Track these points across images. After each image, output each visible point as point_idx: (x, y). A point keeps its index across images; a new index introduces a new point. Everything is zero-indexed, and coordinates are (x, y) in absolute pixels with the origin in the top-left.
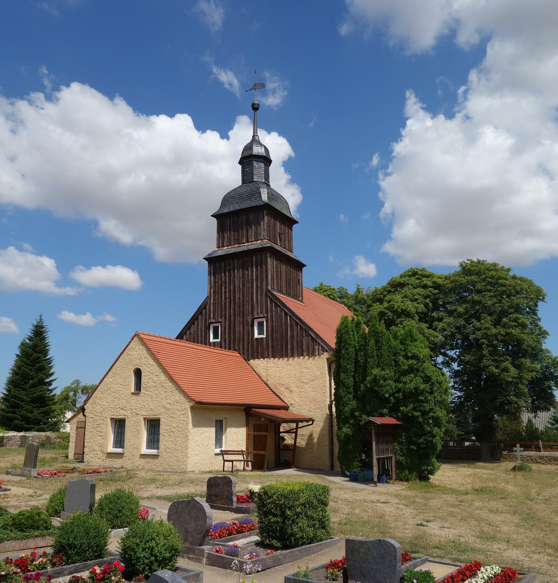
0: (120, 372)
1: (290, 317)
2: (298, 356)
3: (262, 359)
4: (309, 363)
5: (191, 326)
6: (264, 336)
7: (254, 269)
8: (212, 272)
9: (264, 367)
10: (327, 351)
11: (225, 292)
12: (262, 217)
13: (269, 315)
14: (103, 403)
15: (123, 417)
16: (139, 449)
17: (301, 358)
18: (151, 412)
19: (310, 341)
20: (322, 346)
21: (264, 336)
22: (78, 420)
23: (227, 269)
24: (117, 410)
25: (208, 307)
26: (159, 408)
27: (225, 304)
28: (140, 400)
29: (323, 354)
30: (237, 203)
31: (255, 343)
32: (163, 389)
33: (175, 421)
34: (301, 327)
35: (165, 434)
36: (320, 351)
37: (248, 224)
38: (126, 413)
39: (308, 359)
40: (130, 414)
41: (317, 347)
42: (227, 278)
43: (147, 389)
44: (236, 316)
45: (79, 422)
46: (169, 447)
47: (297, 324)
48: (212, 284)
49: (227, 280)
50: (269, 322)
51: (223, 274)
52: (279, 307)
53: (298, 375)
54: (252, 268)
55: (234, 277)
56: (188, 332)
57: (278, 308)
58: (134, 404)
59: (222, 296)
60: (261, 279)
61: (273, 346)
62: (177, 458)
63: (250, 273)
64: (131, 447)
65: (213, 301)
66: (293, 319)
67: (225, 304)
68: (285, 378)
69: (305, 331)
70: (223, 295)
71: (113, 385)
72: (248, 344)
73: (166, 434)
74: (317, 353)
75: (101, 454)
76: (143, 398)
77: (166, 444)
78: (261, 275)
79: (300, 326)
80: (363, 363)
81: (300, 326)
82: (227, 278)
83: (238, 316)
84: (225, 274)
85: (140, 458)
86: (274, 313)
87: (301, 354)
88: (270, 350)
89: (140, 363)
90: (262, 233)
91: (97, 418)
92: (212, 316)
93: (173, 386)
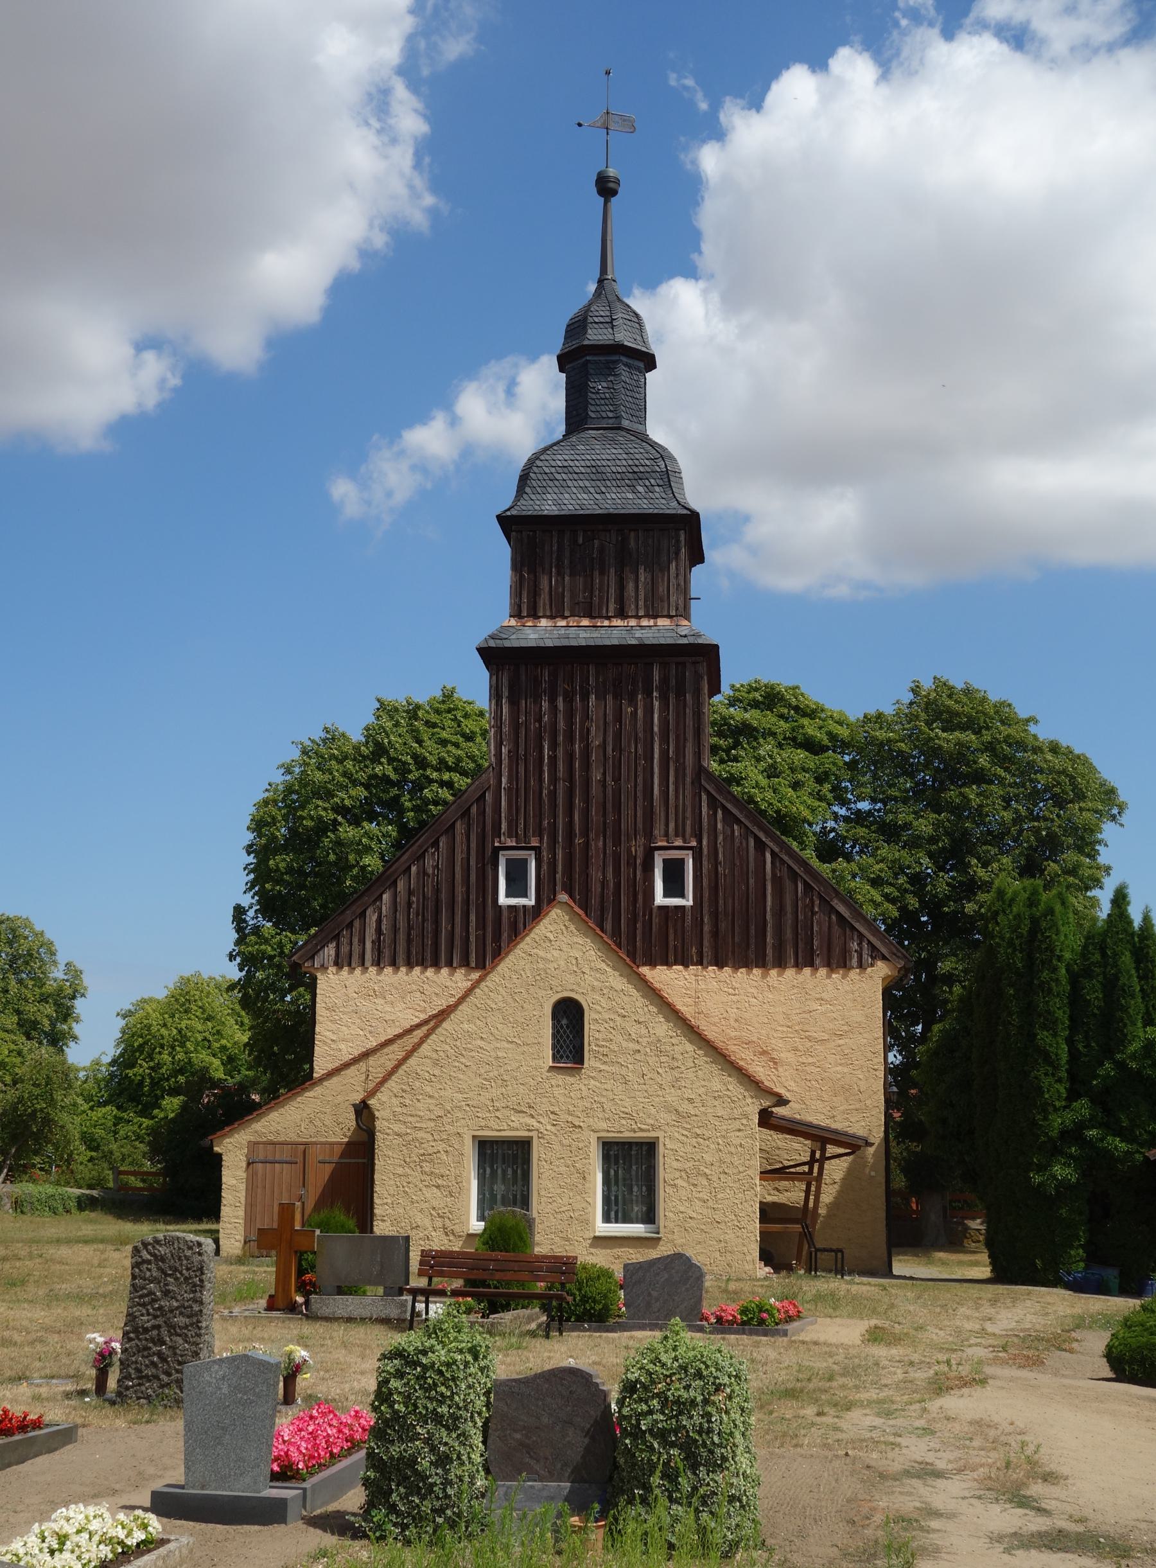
0: (501, 1004)
1: (773, 853)
2: (798, 966)
3: (680, 968)
4: (830, 987)
5: (426, 850)
6: (688, 902)
7: (656, 704)
8: (506, 693)
9: (687, 989)
10: (884, 958)
11: (553, 760)
12: (672, 549)
13: (705, 842)
14: (442, 1093)
15: (526, 1134)
16: (587, 1222)
17: (807, 971)
18: (624, 1122)
19: (836, 929)
20: (869, 942)
21: (688, 902)
22: (252, 1139)
23: (560, 690)
24: (498, 1114)
25: (489, 797)
26: (653, 1111)
27: (553, 794)
28: (583, 1088)
29: (872, 965)
30: (584, 489)
31: (655, 920)
32: (663, 1059)
33: (712, 1146)
34: (807, 885)
35: (676, 1182)
36: (865, 956)
37: (625, 561)
38: (535, 1124)
39: (829, 976)
40: (549, 1127)
41: (855, 946)
42: (561, 717)
43: (605, 1059)
44: (592, 835)
45: (258, 1143)
46: (694, 1215)
47: (794, 876)
48: (505, 729)
49: (561, 725)
50: (705, 863)
51: (545, 705)
52: (739, 822)
53: (797, 1018)
54: (648, 694)
55: (586, 716)
56: (414, 869)
57: (736, 827)
58: (562, 1099)
59: (541, 772)
60: (677, 737)
61: (715, 934)
62: (723, 1244)
63: (640, 712)
64: (559, 1216)
65: (510, 781)
66: (783, 862)
67: (553, 794)
68: (757, 1025)
69: (821, 897)
70: (546, 769)
71: (479, 1042)
72: (633, 920)
73: (679, 1182)
74: (855, 962)
75: (444, 1237)
76: (592, 1082)
77: (682, 1209)
78: (677, 724)
79: (806, 884)
80: (1099, 1008)
81: (806, 884)
82: (561, 717)
83: (597, 836)
84: (553, 701)
85: (592, 1246)
86: (720, 838)
87: (805, 960)
88: (706, 943)
89: (579, 985)
90: (673, 599)
91: (420, 1134)
92: (504, 826)
93: (701, 1052)
